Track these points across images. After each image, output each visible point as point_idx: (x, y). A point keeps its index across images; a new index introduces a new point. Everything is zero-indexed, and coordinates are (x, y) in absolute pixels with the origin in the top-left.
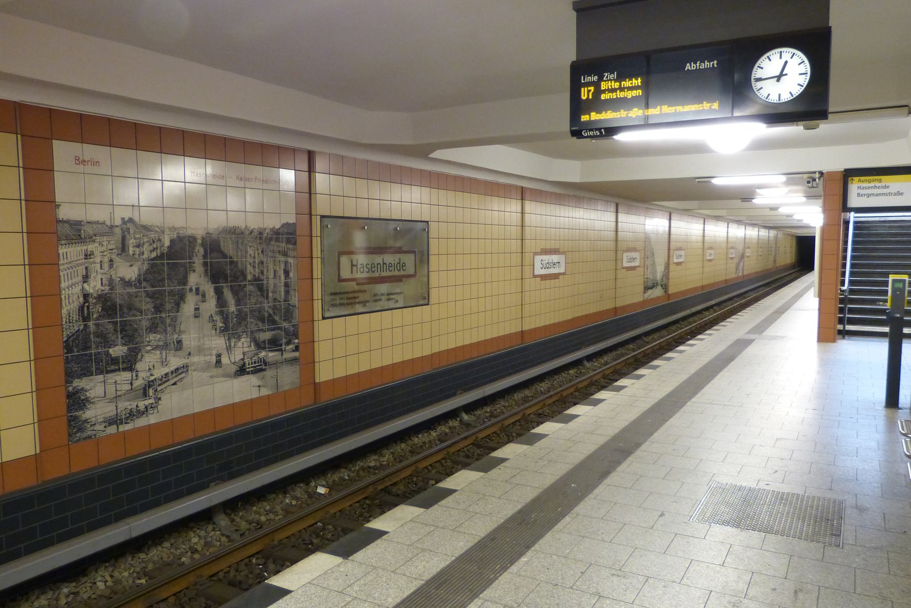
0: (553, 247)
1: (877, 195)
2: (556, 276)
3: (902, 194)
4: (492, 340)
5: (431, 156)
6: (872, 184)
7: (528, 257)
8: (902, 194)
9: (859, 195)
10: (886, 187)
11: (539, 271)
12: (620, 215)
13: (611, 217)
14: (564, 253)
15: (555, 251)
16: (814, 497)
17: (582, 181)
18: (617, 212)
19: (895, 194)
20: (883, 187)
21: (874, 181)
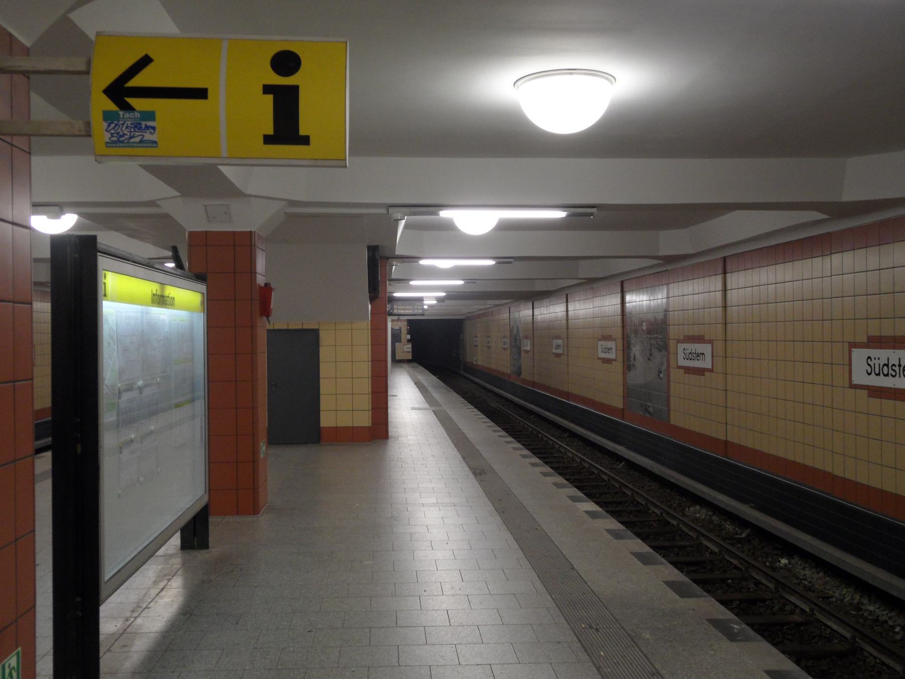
7: (565, 353)
18: (567, 302)
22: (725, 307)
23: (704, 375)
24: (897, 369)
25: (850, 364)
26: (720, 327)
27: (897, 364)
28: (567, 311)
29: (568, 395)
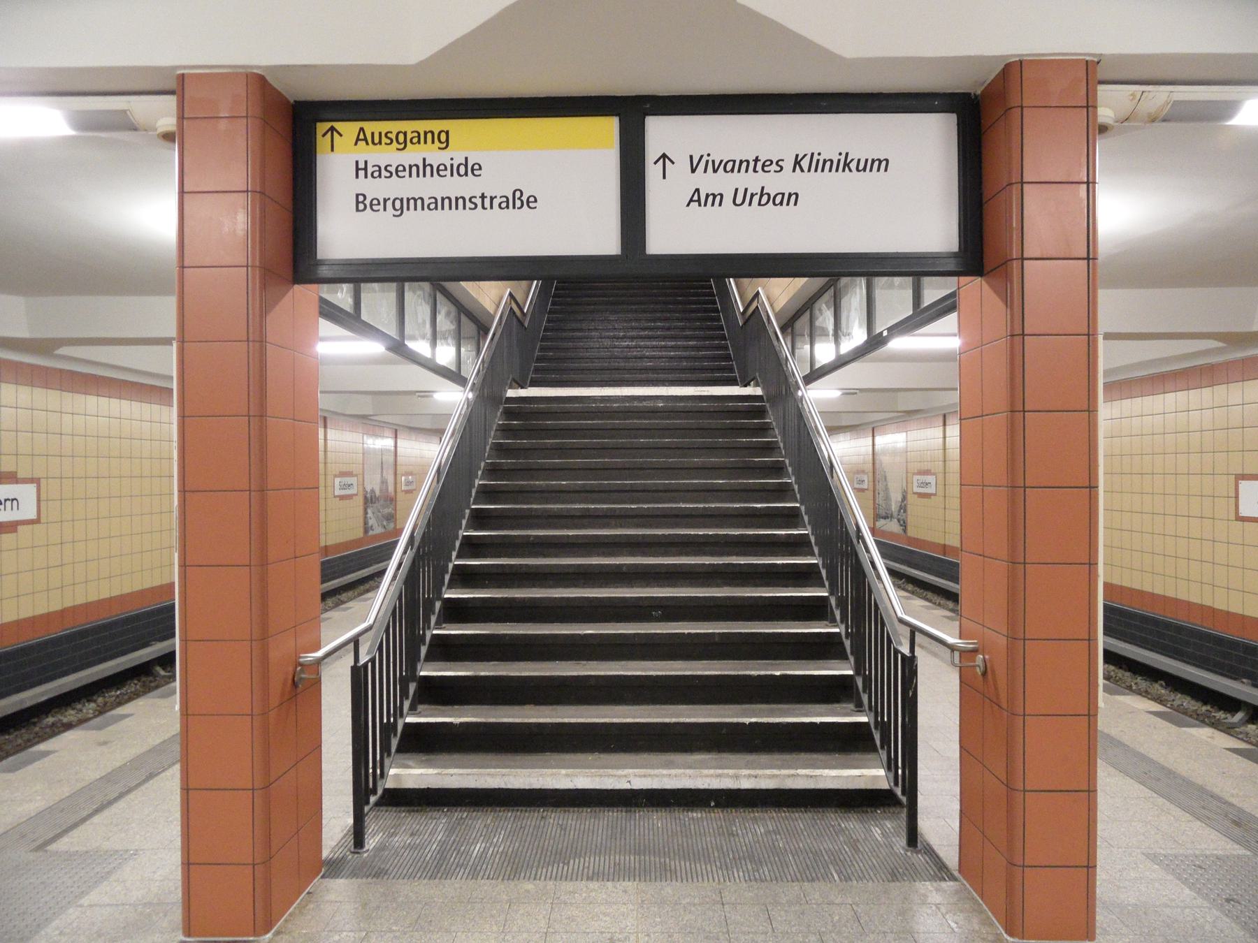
1: (437, 204)
3: (531, 202)
5: (57, 352)
6: (413, 155)
7: (941, 493)
8: (531, 202)
9: (361, 202)
10: (470, 169)
12: (329, 431)
16: (764, 429)
18: (945, 425)
19: (507, 204)
20: (455, 170)
21: (419, 138)
22: (945, 449)
23: (16, 531)
25: (39, 500)
26: (941, 463)
28: (945, 437)
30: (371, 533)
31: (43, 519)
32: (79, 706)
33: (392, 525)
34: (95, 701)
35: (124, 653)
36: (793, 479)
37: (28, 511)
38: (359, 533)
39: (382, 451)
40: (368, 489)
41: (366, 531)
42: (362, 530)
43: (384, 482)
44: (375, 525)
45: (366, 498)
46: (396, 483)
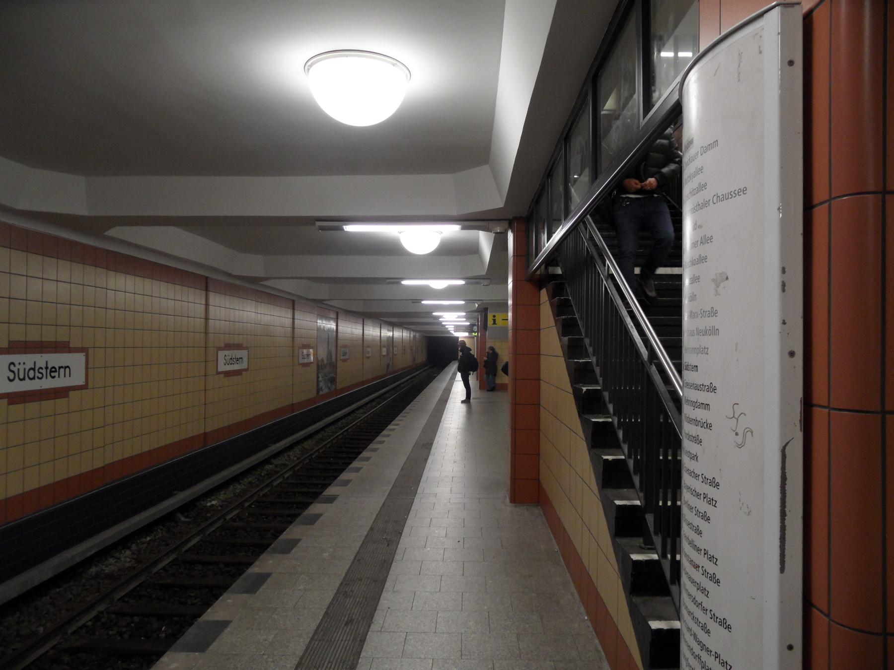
0: (236, 342)
2: (238, 373)
4: (81, 477)
5: (106, 233)
11: (222, 368)
12: (212, 296)
13: (289, 314)
14: (246, 348)
15: (239, 347)
17: (94, 214)
22: (293, 328)
23: (67, 396)
24: (44, 371)
25: (87, 368)
26: (203, 335)
27: (44, 366)
29: (363, 383)
30: (321, 393)
31: (90, 386)
32: (117, 555)
33: (334, 387)
34: (129, 548)
35: (152, 504)
36: (593, 360)
37: (77, 378)
38: (312, 394)
39: (329, 330)
40: (320, 359)
41: (318, 392)
42: (315, 392)
43: (329, 353)
44: (324, 387)
45: (318, 365)
46: (336, 353)
